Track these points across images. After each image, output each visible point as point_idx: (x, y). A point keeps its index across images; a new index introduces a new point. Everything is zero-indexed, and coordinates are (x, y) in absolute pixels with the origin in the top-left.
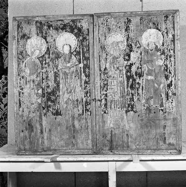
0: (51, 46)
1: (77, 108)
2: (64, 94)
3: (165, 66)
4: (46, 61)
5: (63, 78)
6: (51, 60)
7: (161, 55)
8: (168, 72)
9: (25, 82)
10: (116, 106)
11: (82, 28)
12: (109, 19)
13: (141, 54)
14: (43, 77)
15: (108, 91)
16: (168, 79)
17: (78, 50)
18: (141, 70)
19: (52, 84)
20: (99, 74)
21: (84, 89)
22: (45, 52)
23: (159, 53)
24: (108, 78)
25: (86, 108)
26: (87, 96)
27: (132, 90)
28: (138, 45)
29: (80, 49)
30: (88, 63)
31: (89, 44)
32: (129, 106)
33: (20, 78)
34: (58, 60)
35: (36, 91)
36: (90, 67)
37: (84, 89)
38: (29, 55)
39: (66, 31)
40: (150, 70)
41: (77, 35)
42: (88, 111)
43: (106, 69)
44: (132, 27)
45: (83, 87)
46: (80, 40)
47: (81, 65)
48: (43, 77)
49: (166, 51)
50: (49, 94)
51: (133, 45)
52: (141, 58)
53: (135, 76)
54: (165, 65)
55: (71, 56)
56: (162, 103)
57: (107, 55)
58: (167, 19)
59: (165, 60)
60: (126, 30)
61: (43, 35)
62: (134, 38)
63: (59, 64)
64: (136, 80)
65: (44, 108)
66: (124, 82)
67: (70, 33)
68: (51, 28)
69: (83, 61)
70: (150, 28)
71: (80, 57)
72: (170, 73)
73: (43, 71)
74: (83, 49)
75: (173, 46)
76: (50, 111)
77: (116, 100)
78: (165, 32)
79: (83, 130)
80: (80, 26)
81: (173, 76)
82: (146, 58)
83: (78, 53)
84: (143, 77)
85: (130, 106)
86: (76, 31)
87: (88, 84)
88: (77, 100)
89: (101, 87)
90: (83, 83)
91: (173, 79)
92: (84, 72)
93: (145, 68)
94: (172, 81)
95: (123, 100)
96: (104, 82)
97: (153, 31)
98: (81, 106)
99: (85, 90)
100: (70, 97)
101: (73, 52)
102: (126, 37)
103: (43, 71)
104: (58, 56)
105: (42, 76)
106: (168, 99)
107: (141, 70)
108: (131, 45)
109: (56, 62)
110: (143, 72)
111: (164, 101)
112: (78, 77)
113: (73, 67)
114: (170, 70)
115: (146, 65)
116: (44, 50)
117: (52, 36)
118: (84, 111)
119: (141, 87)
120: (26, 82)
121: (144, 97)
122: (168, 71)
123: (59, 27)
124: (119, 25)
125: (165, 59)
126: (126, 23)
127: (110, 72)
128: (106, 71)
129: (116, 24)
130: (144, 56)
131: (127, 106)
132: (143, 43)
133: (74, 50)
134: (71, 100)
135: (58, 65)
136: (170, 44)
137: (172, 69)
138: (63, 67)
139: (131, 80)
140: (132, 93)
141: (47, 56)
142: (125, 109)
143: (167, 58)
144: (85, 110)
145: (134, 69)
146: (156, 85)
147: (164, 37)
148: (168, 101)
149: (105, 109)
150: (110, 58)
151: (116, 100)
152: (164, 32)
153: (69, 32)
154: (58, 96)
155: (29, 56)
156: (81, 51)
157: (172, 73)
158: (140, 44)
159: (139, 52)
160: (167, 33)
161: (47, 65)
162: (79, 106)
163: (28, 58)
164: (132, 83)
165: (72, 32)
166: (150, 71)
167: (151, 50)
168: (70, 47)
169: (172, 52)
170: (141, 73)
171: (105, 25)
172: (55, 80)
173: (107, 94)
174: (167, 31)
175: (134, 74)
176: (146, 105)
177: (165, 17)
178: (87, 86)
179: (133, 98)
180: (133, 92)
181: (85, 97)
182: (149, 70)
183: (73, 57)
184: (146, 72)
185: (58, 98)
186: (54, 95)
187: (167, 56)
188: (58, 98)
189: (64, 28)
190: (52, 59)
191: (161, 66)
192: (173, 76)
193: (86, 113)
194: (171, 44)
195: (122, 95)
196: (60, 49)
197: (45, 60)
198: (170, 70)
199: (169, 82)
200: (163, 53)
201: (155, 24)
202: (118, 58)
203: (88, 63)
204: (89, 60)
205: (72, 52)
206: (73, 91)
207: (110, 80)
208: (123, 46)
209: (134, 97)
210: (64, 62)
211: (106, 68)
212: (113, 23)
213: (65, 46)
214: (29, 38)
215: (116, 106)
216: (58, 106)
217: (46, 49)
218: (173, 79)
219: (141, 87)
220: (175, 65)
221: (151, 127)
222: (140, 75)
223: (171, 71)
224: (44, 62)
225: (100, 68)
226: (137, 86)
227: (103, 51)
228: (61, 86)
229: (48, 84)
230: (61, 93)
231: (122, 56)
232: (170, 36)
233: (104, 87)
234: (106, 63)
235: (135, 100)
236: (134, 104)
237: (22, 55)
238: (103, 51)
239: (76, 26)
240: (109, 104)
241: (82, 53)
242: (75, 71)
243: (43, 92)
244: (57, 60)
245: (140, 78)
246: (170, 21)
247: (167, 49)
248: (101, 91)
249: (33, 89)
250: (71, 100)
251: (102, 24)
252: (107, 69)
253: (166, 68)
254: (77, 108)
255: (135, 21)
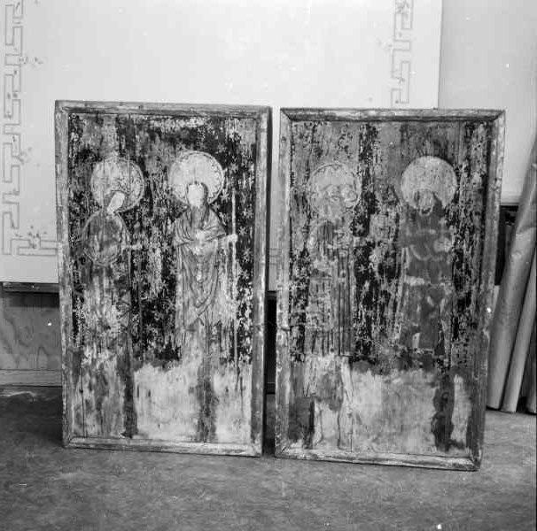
0: (155, 186)
1: (218, 345)
2: (185, 308)
3: (458, 253)
4: (141, 223)
5: (183, 268)
6: (154, 222)
7: (448, 225)
8: (462, 271)
9: (87, 272)
10: (325, 345)
11: (239, 141)
12: (319, 126)
13: (397, 220)
14: (133, 264)
15: (308, 308)
16: (461, 288)
17: (225, 197)
18: (395, 261)
19: (157, 284)
20: (287, 266)
21: (237, 299)
22: (139, 199)
23: (443, 222)
24: (309, 275)
25: (239, 344)
26: (243, 316)
27: (367, 309)
28: (391, 198)
29: (230, 196)
30: (248, 232)
31: (253, 185)
32: (358, 347)
33: (76, 262)
34: (173, 221)
35: (116, 296)
36: (255, 243)
37: (237, 299)
38: (97, 205)
39: (195, 149)
40: (417, 260)
41: (225, 161)
42: (245, 352)
43: (304, 253)
44: (379, 150)
45: (235, 293)
46: (231, 172)
47: (233, 238)
48: (133, 264)
49: (463, 215)
50: (150, 306)
51: (378, 197)
52: (397, 230)
53: (377, 276)
54: (455, 251)
55: (207, 213)
56: (442, 344)
57: (309, 217)
58: (471, 132)
59: (458, 238)
60: (362, 157)
61: (134, 153)
62: (381, 177)
63: (176, 231)
64: (379, 285)
65: (135, 341)
66: (349, 288)
67: (207, 154)
68: (157, 138)
69: (237, 228)
70: (426, 155)
71: (230, 216)
72: (469, 273)
73: (134, 247)
74: (238, 198)
75: (480, 204)
76: (151, 347)
77: (326, 330)
78: (464, 167)
79: (230, 398)
80: (232, 136)
81: (475, 281)
82: (408, 233)
83: (224, 207)
84: (398, 277)
85: (362, 348)
86: (221, 149)
87: (247, 286)
88: (219, 325)
89: (291, 297)
90: (235, 284)
91: (474, 287)
92: (240, 256)
93: (408, 255)
94: (469, 294)
95: (344, 331)
96: (299, 284)
97: (432, 162)
98: (228, 339)
99: (239, 302)
100: (202, 317)
101: (214, 203)
102: (360, 174)
103: (134, 247)
104: (176, 211)
105: (132, 261)
106: (456, 336)
107: (395, 261)
108: (373, 196)
109: (169, 227)
110: (400, 265)
111: (446, 341)
112: (223, 267)
113: (210, 241)
114: (467, 266)
115: (407, 249)
116: (137, 194)
117: (159, 159)
118: (236, 351)
119: (391, 303)
120: (91, 272)
121: (397, 328)
122: (463, 267)
123: (179, 136)
124: (344, 143)
125: (458, 236)
126: (364, 138)
127: (317, 261)
128: (307, 259)
129: (337, 139)
130: (405, 225)
131: (353, 346)
132: (404, 192)
133: (216, 198)
134: (204, 322)
135: (173, 233)
136: (473, 198)
137: (474, 261)
138: (187, 241)
139: (367, 285)
140: (367, 317)
141: (145, 210)
142: (348, 354)
143: (463, 235)
144: (239, 350)
145: (375, 257)
146: (429, 299)
147: (458, 181)
148: (457, 341)
149: (298, 352)
150: (315, 226)
151: (326, 330)
152: (461, 166)
153: (203, 150)
154: (170, 312)
155: (100, 207)
156: (234, 201)
157: (473, 271)
158: (395, 195)
159: (393, 214)
160: (468, 170)
161: (144, 232)
162: (223, 340)
163: (97, 213)
164: (371, 292)
165: (211, 150)
166: (416, 266)
167: (424, 212)
168: (206, 189)
169: (477, 218)
170: (395, 268)
171: (309, 139)
172: (165, 273)
173: (304, 314)
174: (470, 166)
175: (376, 269)
176: (400, 347)
177: (467, 126)
178: (244, 292)
179: (369, 328)
180: (371, 313)
181: (238, 317)
182: (414, 261)
183: (212, 214)
184: (407, 266)
185: (171, 316)
186: (160, 309)
187: (463, 229)
188: (171, 316)
189: (191, 139)
190: (158, 217)
191: (445, 255)
192: (475, 281)
193: (239, 356)
194: (477, 200)
195: (341, 319)
196: (179, 192)
197: (140, 220)
198: (467, 266)
199: (463, 294)
200: (454, 221)
201: (440, 145)
202: (337, 226)
203: (251, 232)
204: (254, 225)
205: (209, 203)
206: (208, 301)
207: (314, 282)
208: (352, 198)
209: (373, 326)
210: (189, 228)
211: (305, 250)
212: (329, 136)
213: (192, 187)
214: (98, 158)
215: (325, 345)
216: (170, 337)
217: (143, 190)
218: (474, 287)
219: (391, 303)
220: (481, 254)
221: (409, 398)
222: (391, 273)
223: (470, 269)
224: (137, 226)
225: (291, 250)
226: (382, 300)
227: (300, 207)
228: (179, 289)
229: (146, 281)
230: (179, 305)
231: (349, 222)
232: (477, 178)
233: (299, 297)
234: (307, 238)
235: (375, 333)
236: (370, 342)
237: (79, 202)
238: (300, 207)
239: (222, 135)
240: (308, 339)
241: (235, 210)
242: (215, 251)
243: (133, 298)
244: (169, 222)
245: (389, 281)
246: (480, 138)
247: (466, 211)
248: (290, 306)
249: (109, 291)
250: (202, 323)
251: (301, 137)
252: (308, 254)
253: (458, 260)
254: (218, 345)
255: (388, 135)
